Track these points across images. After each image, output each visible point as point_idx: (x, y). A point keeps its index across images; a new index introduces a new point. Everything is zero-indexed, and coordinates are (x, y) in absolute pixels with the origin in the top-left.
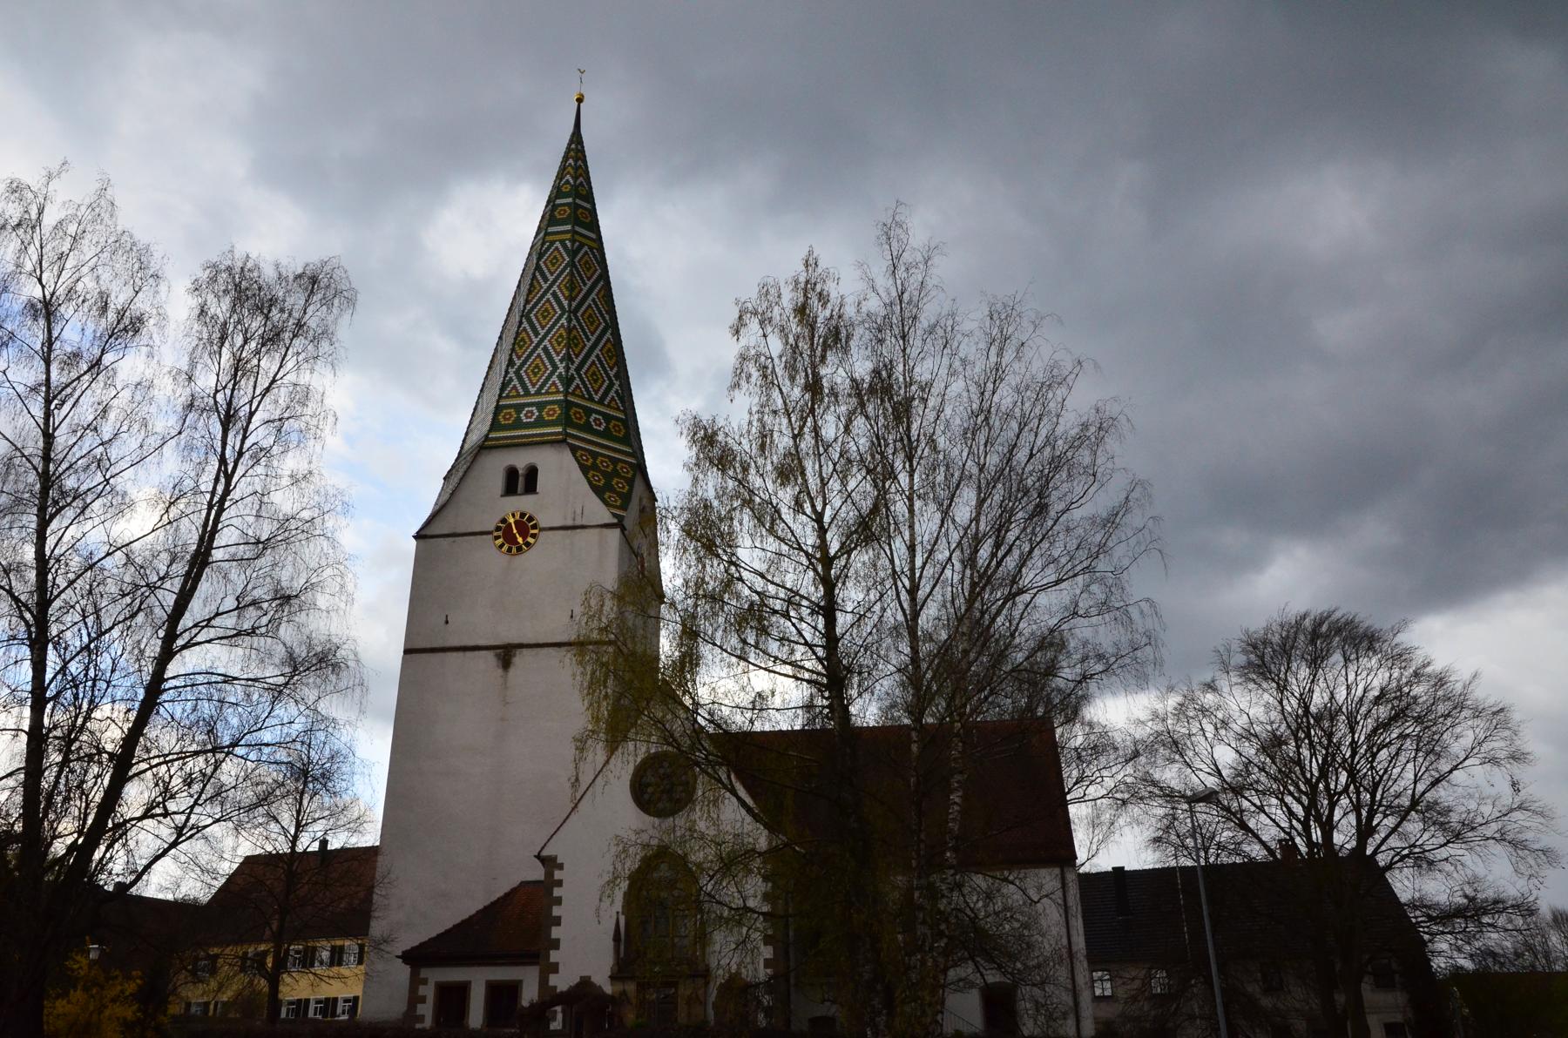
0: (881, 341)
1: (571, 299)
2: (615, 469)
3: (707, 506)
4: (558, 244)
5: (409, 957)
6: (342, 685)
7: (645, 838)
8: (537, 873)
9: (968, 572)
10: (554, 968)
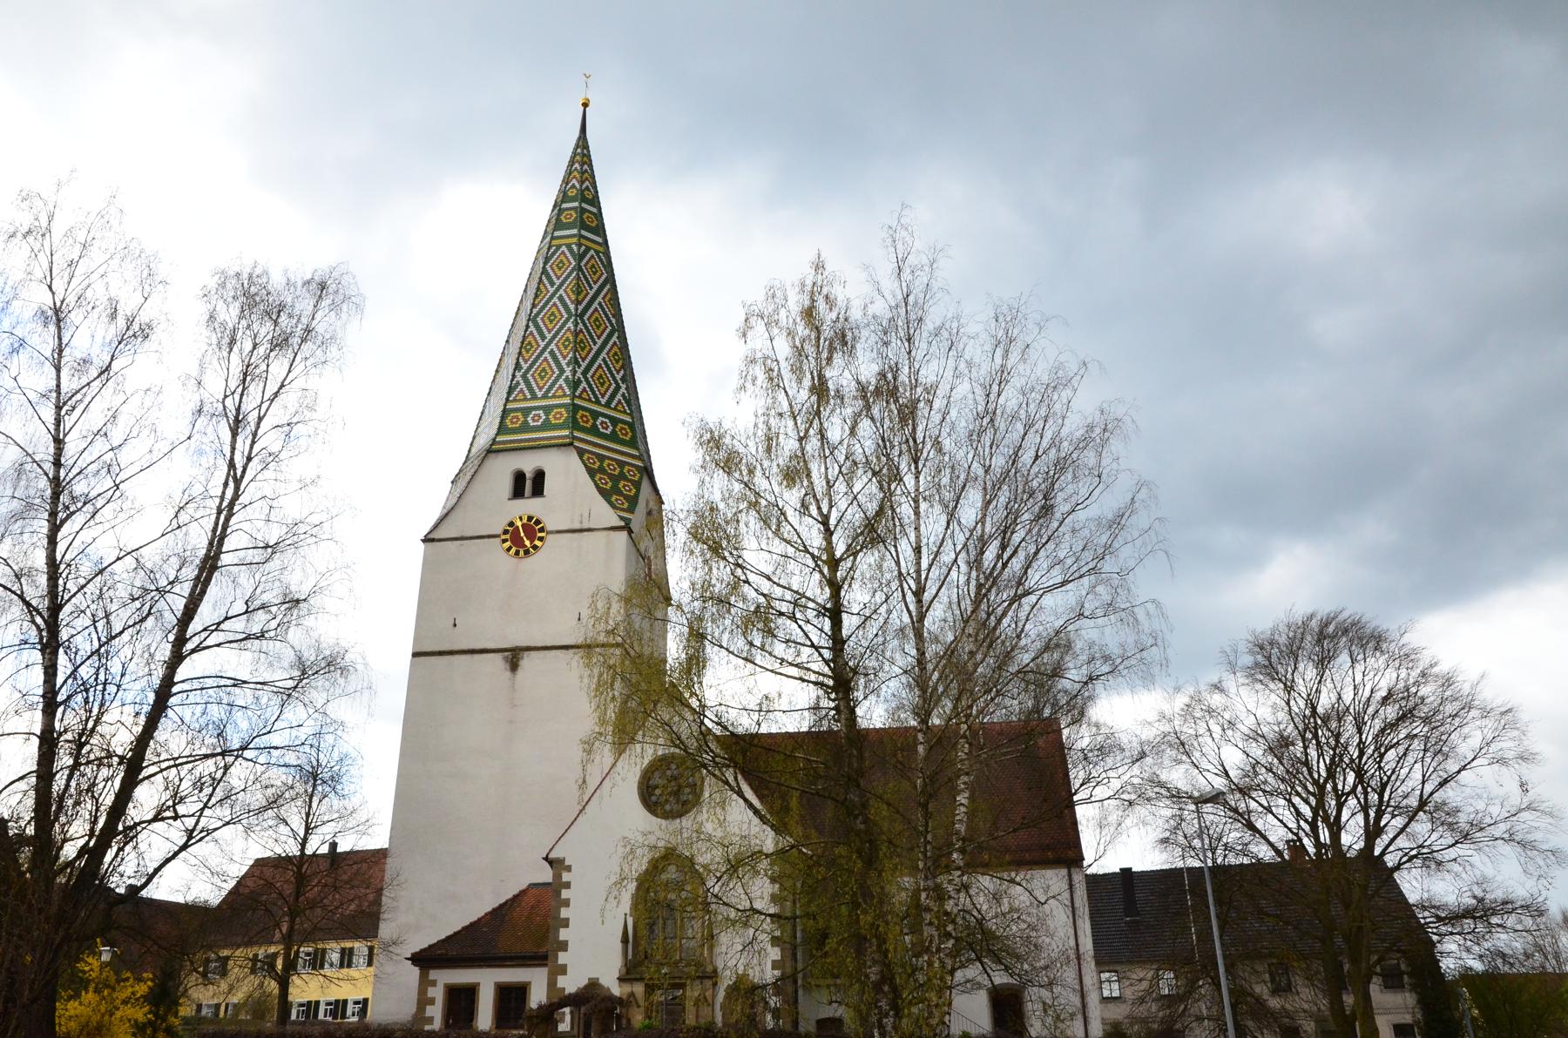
0: (886, 344)
1: (578, 303)
2: (622, 473)
4: (564, 248)
5: (416, 959)
6: (350, 689)
7: (652, 840)
8: (546, 875)
9: (974, 574)
10: (563, 970)
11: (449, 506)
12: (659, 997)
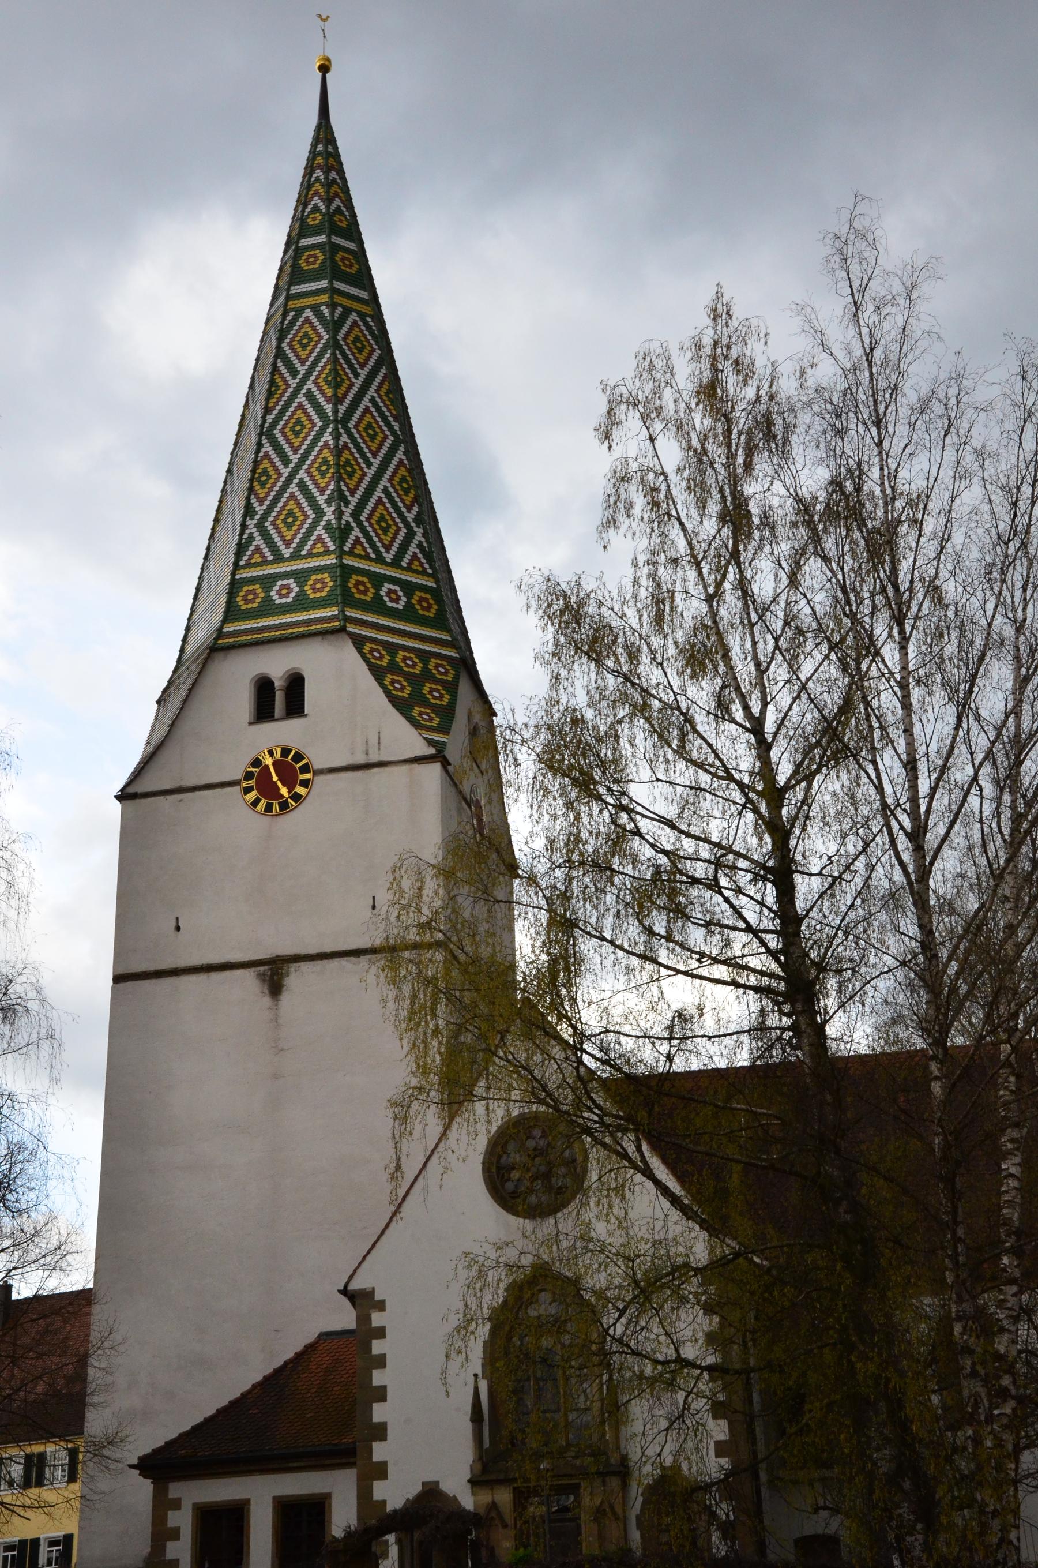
0: (841, 433)
1: (337, 401)
2: (392, 662)
3: (577, 721)
4: (308, 313)
5: (147, 1466)
6: (20, 1040)
7: (511, 1255)
8: (345, 1318)
9: (1007, 798)
10: (381, 1471)
11: (156, 740)
12: (536, 1509)
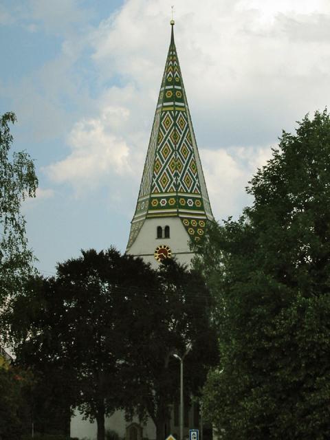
1: (175, 144)
